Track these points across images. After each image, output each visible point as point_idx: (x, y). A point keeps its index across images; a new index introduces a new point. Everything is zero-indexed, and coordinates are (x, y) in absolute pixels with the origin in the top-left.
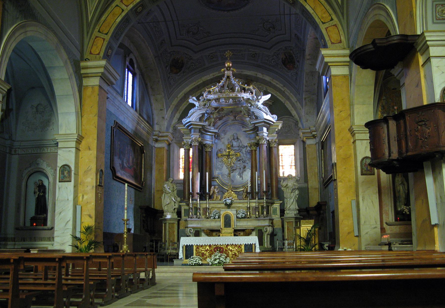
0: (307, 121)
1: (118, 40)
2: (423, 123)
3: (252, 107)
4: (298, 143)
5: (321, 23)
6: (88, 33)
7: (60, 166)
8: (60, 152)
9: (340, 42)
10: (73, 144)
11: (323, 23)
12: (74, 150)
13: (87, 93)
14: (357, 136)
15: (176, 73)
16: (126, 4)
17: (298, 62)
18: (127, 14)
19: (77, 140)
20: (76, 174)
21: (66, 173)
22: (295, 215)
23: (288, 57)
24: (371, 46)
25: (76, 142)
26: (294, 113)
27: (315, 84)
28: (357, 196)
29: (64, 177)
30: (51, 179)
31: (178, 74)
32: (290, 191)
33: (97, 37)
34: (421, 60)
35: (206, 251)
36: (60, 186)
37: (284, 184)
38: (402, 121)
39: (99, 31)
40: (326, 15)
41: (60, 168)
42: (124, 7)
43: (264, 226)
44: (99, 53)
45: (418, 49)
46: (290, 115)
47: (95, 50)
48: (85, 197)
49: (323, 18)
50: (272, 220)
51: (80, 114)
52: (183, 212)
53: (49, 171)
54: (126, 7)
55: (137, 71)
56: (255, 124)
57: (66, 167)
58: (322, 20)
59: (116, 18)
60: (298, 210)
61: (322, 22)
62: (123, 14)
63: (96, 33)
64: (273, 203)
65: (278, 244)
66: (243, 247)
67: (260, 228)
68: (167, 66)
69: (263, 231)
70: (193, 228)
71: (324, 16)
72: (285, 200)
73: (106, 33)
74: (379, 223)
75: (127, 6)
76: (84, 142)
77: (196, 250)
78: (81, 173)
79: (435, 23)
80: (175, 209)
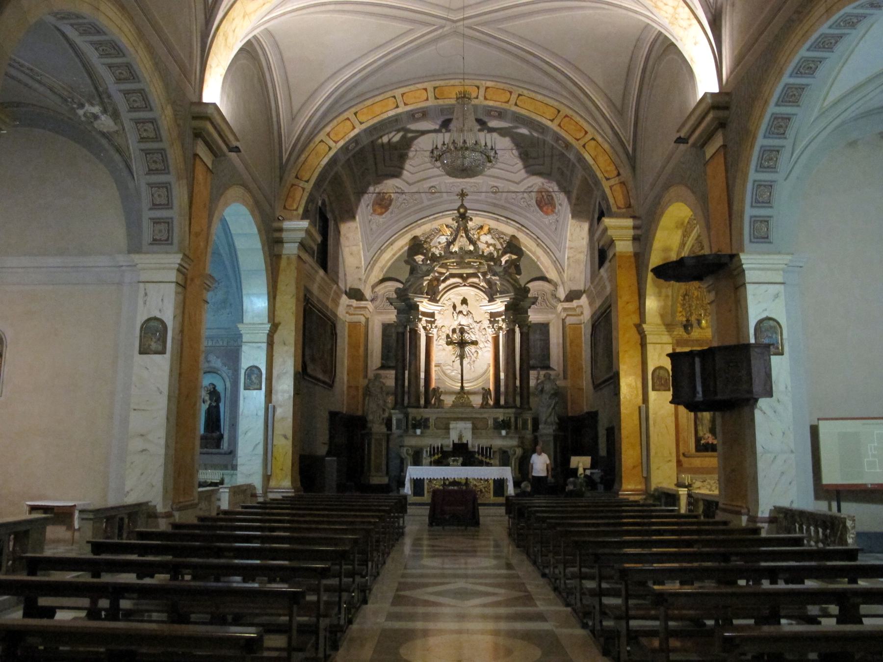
5: (604, 179)
7: (246, 368)
11: (607, 179)
15: (381, 214)
16: (335, 139)
17: (560, 205)
18: (336, 154)
19: (181, 268)
21: (253, 377)
22: (554, 431)
23: (545, 197)
25: (178, 270)
29: (252, 383)
31: (384, 216)
36: (246, 395)
41: (246, 370)
42: (332, 144)
44: (297, 208)
49: (607, 171)
52: (394, 422)
54: (334, 144)
57: (253, 370)
58: (606, 175)
60: (558, 424)
61: (605, 177)
62: (331, 154)
66: (491, 482)
68: (368, 205)
69: (510, 453)
70: (411, 447)
71: (608, 169)
74: (674, 454)
75: (336, 142)
77: (428, 484)
79: (754, 242)
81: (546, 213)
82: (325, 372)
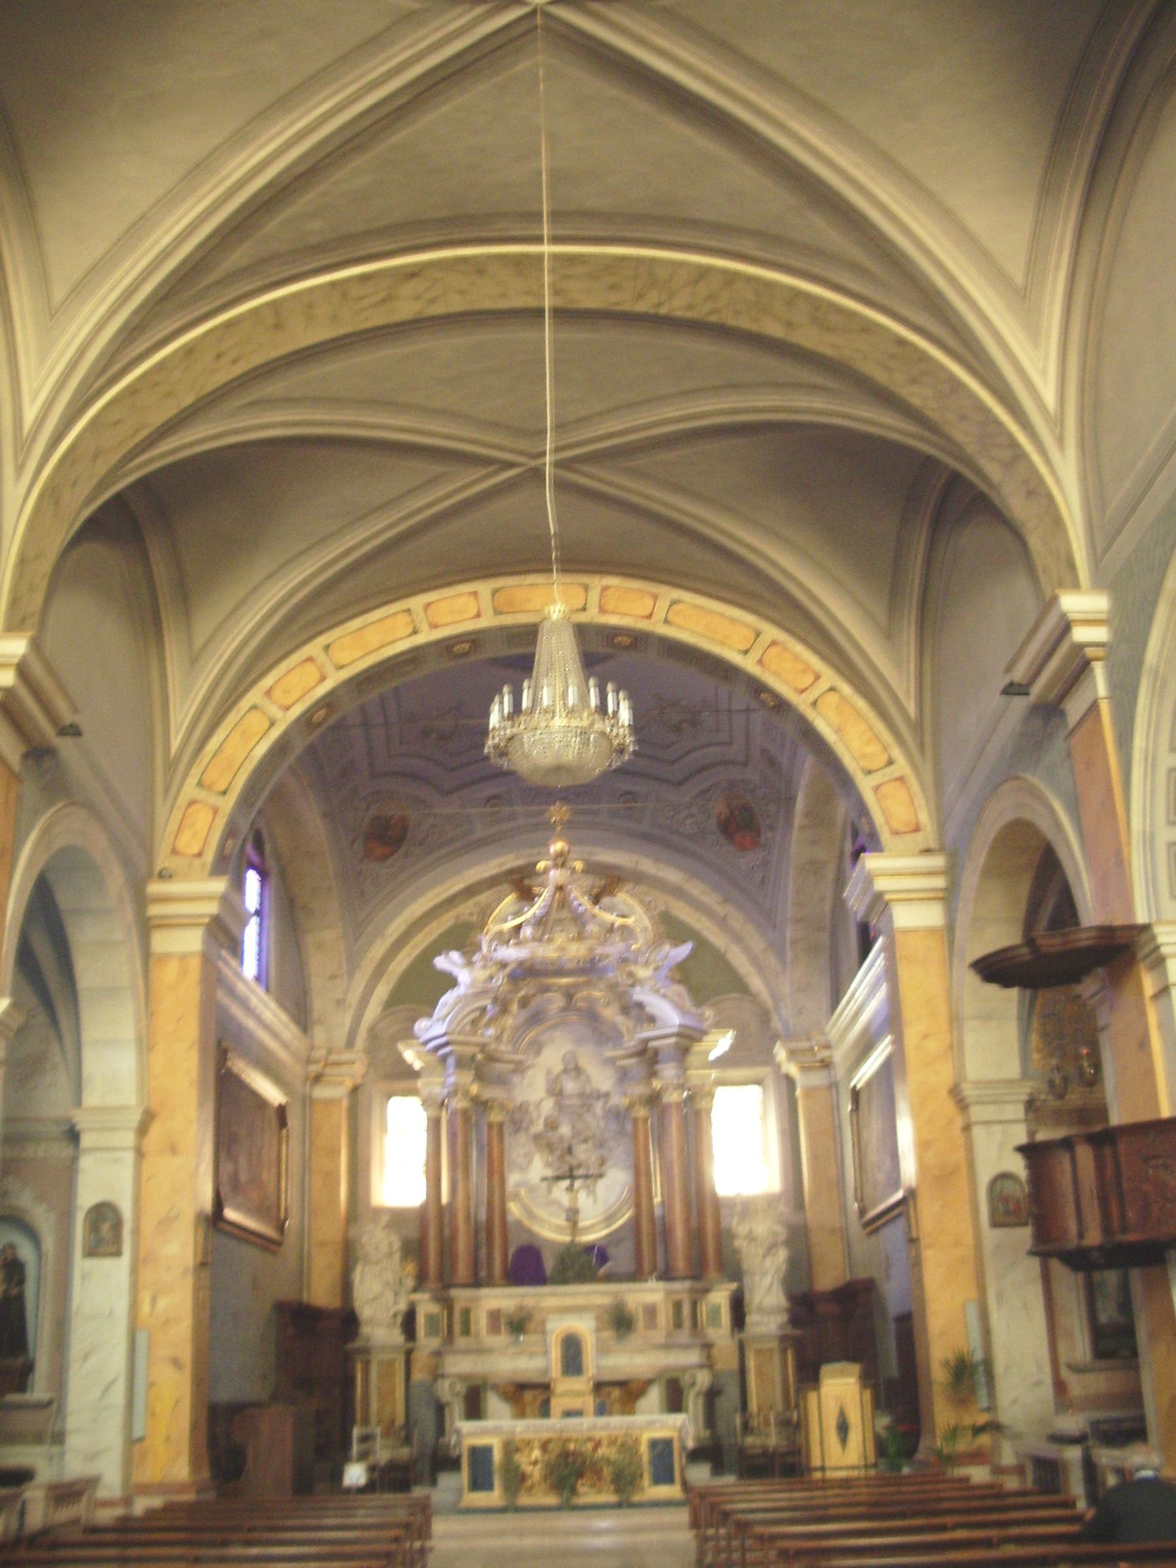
0: (800, 1012)
1: (253, 804)
2: (1160, 1162)
3: (638, 989)
4: (770, 1082)
6: (167, 790)
8: (86, 1163)
9: (917, 829)
10: (128, 1139)
12: (129, 1157)
13: (167, 974)
14: (976, 1113)
15: (384, 858)
20: (136, 1231)
21: (105, 1228)
24: (1024, 950)
26: (756, 983)
27: (822, 900)
28: (982, 1289)
30: (49, 1243)
32: (761, 1252)
33: (192, 803)
34: (1149, 985)
35: (535, 1463)
37: (741, 1229)
38: (1107, 1151)
39: (200, 784)
40: (873, 748)
43: (685, 1369)
45: (1141, 955)
46: (741, 987)
47: (190, 843)
48: (163, 1303)
50: (707, 1347)
51: (145, 1045)
53: (43, 1218)
55: (271, 863)
56: (646, 1041)
59: (254, 743)
63: (190, 789)
64: (707, 1291)
65: (483, 1273)
67: (674, 1375)
70: (462, 1377)
72: (747, 1280)
73: (223, 788)
76: (156, 1129)
78: (149, 1224)
80: (395, 1315)
81: (742, 848)
82: (260, 1210)
